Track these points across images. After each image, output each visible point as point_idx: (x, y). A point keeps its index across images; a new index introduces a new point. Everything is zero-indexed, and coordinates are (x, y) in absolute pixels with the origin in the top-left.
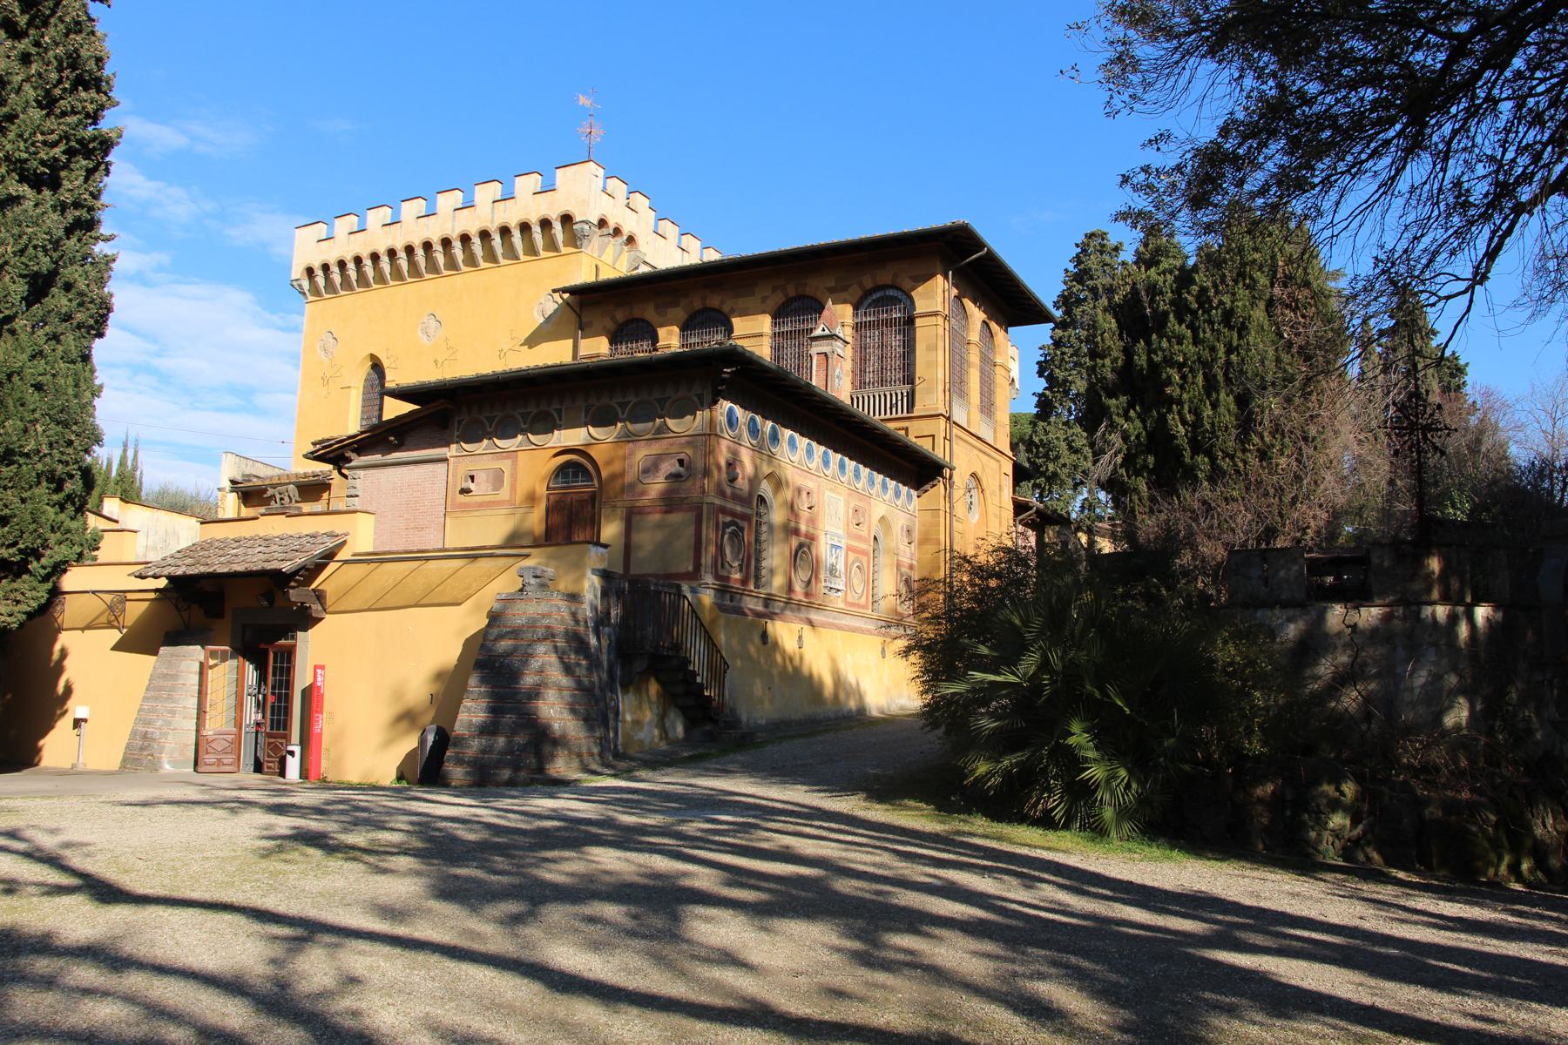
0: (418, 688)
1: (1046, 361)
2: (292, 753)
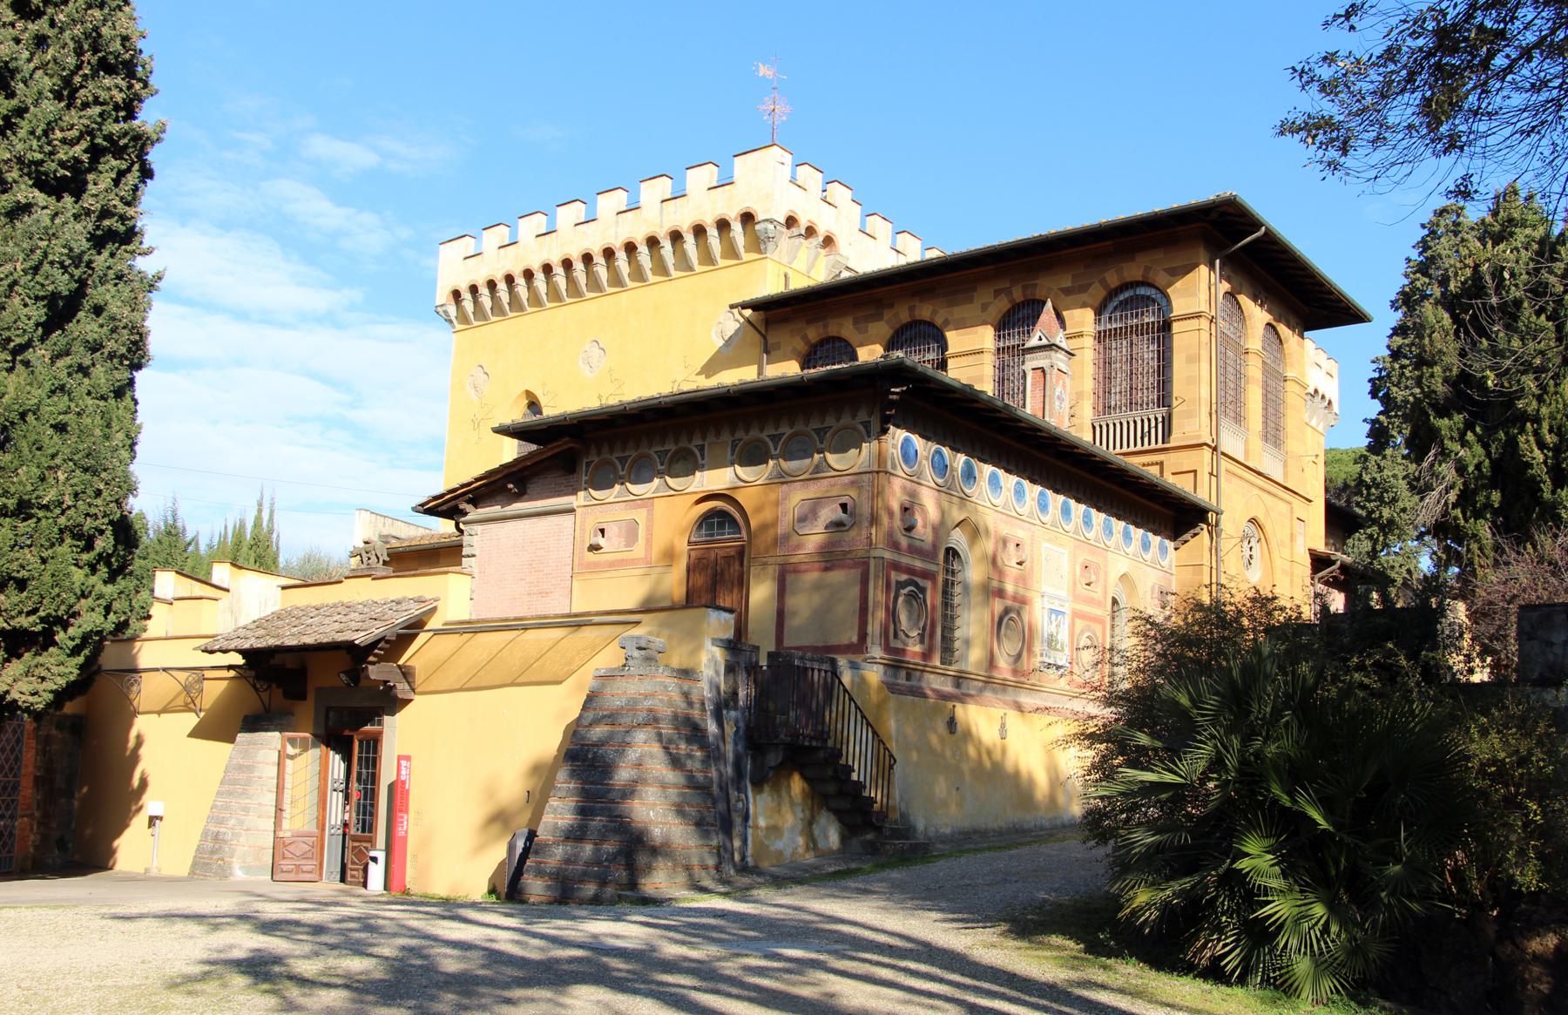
0: (512, 786)
1: (1380, 378)
2: (375, 859)
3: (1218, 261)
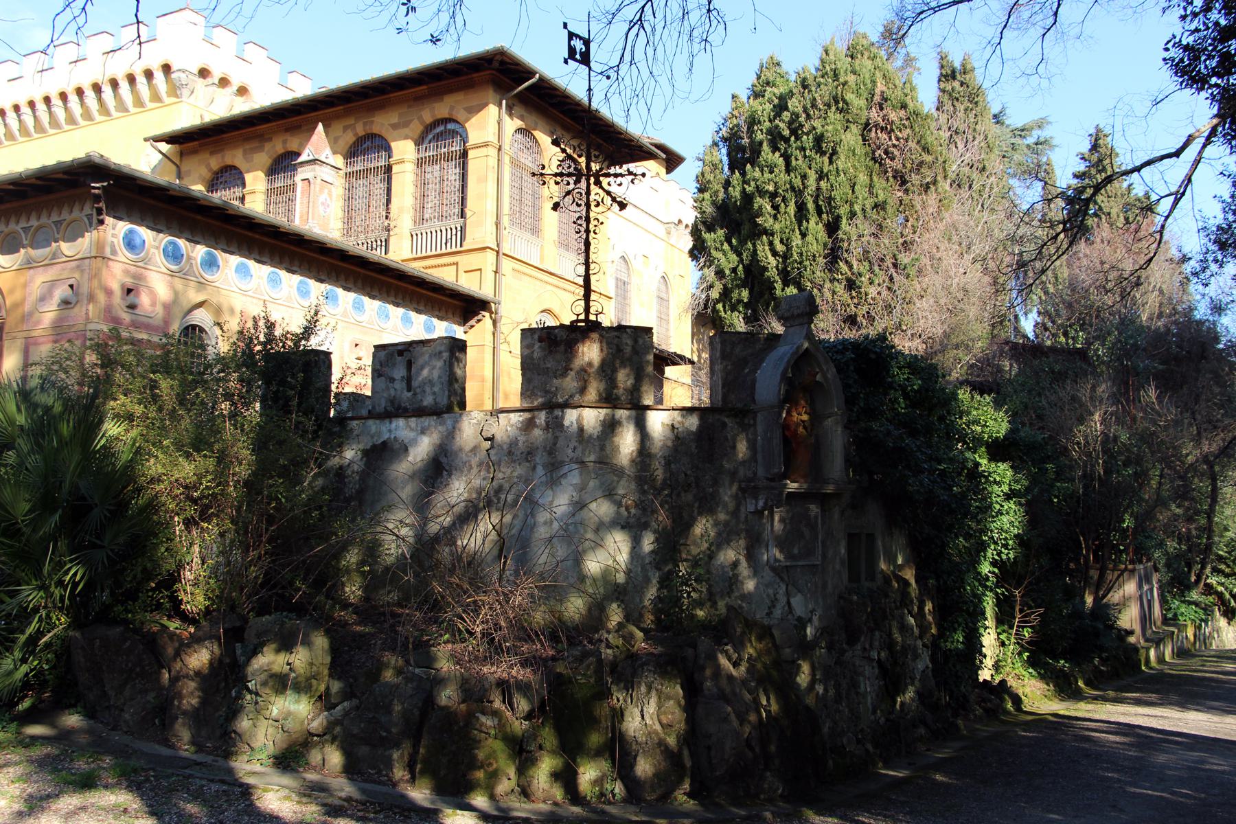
3: (504, 102)
